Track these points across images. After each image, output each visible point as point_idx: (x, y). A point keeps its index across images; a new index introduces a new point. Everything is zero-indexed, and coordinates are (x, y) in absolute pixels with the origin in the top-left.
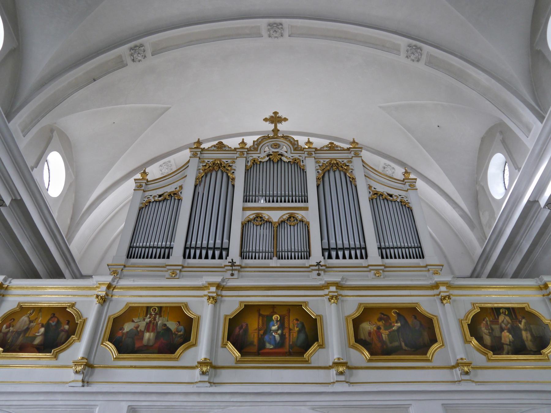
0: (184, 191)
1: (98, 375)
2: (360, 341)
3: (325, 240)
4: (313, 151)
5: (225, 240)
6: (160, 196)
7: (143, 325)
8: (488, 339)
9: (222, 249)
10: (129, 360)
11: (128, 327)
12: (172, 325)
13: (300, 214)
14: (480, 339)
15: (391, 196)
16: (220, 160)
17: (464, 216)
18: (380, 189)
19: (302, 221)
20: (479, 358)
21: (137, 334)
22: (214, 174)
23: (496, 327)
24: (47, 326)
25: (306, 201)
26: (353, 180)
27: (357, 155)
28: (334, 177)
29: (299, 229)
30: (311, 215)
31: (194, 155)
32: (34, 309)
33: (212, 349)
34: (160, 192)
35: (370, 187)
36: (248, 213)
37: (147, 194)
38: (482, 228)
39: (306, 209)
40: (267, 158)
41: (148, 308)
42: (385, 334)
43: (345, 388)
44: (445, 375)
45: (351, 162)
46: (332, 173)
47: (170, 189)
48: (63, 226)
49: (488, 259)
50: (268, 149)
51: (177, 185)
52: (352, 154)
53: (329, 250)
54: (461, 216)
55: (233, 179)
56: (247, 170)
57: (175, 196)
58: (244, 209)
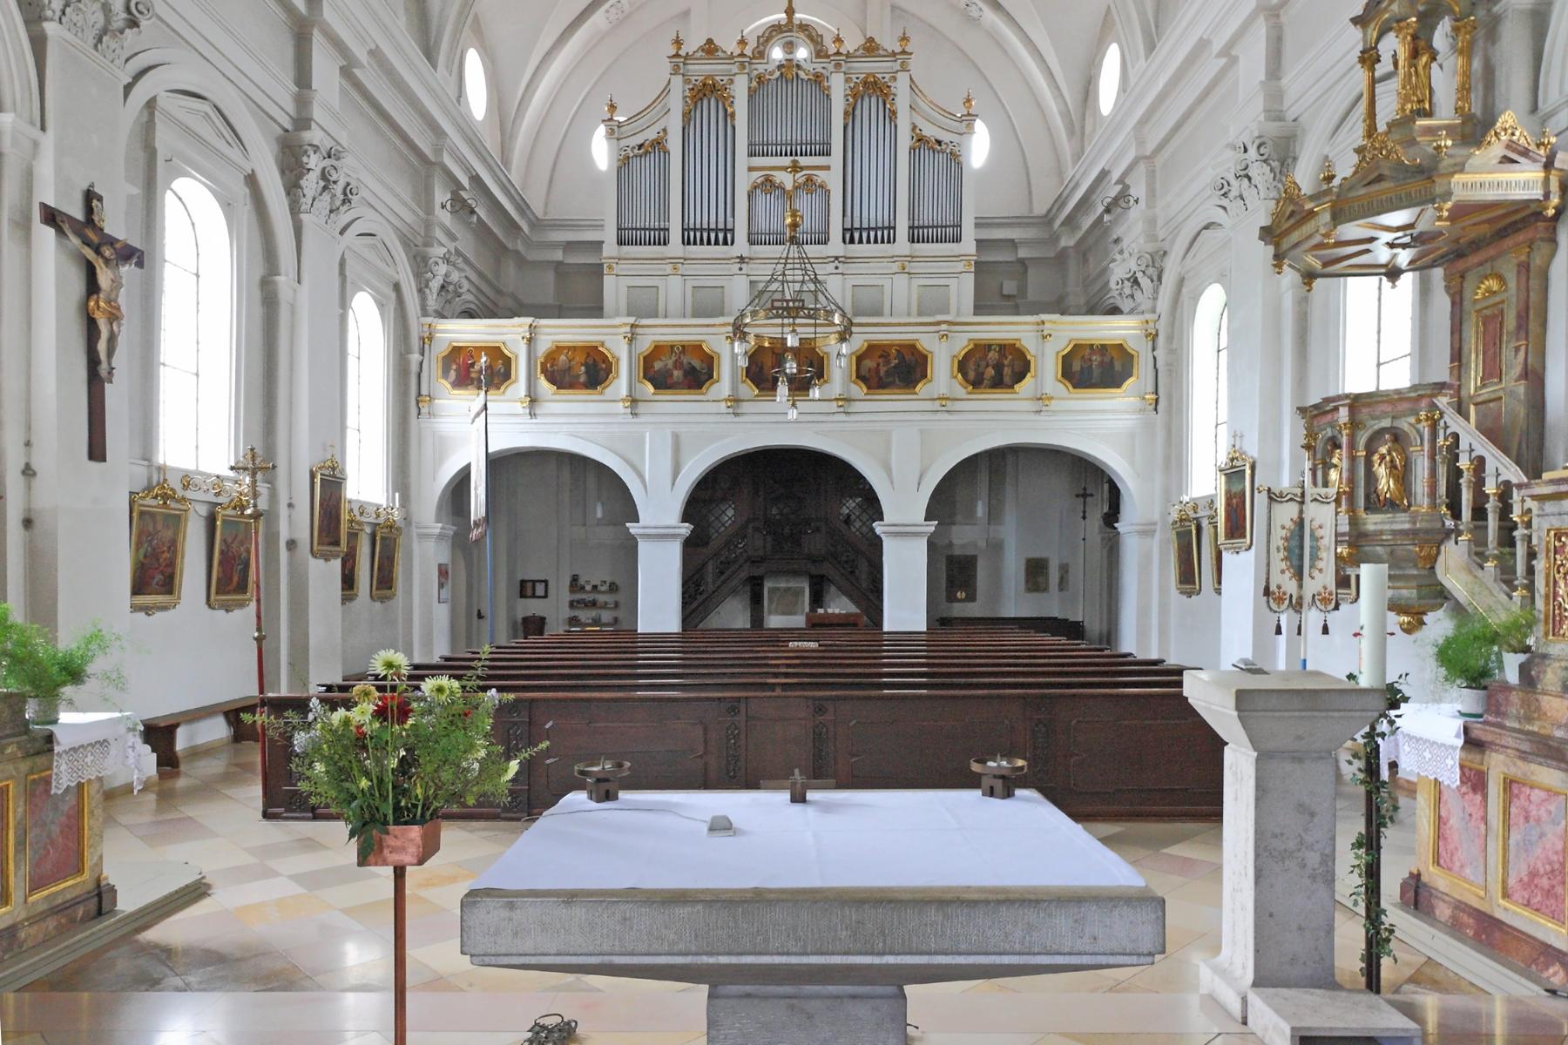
0: (669, 137)
1: (642, 408)
2: (862, 377)
3: (848, 219)
4: (842, 59)
5: (729, 219)
6: (640, 147)
7: (670, 363)
8: (972, 375)
9: (725, 230)
10: (666, 396)
11: (658, 365)
12: (697, 363)
13: (821, 176)
14: (965, 375)
15: (939, 142)
16: (711, 77)
17: (1066, 114)
18: (930, 131)
19: (821, 186)
20: (960, 391)
21: (667, 373)
22: (705, 102)
23: (983, 363)
24: (586, 365)
25: (828, 154)
26: (894, 113)
27: (904, 69)
28: (870, 105)
29: (817, 198)
30: (833, 180)
31: (676, 70)
32: (569, 348)
33: (734, 388)
34: (639, 139)
35: (914, 127)
36: (756, 174)
37: (623, 143)
38: (1082, 140)
39: (828, 168)
40: (778, 74)
41: (672, 347)
42: (883, 370)
43: (843, 417)
44: (928, 405)
45: (895, 79)
46: (866, 100)
47: (651, 135)
48: (491, 144)
49: (1063, 204)
50: (777, 54)
51: (658, 127)
52: (897, 66)
53: (852, 230)
54: (1061, 113)
55: (733, 115)
56: (752, 94)
57: (658, 145)
58: (751, 169)
